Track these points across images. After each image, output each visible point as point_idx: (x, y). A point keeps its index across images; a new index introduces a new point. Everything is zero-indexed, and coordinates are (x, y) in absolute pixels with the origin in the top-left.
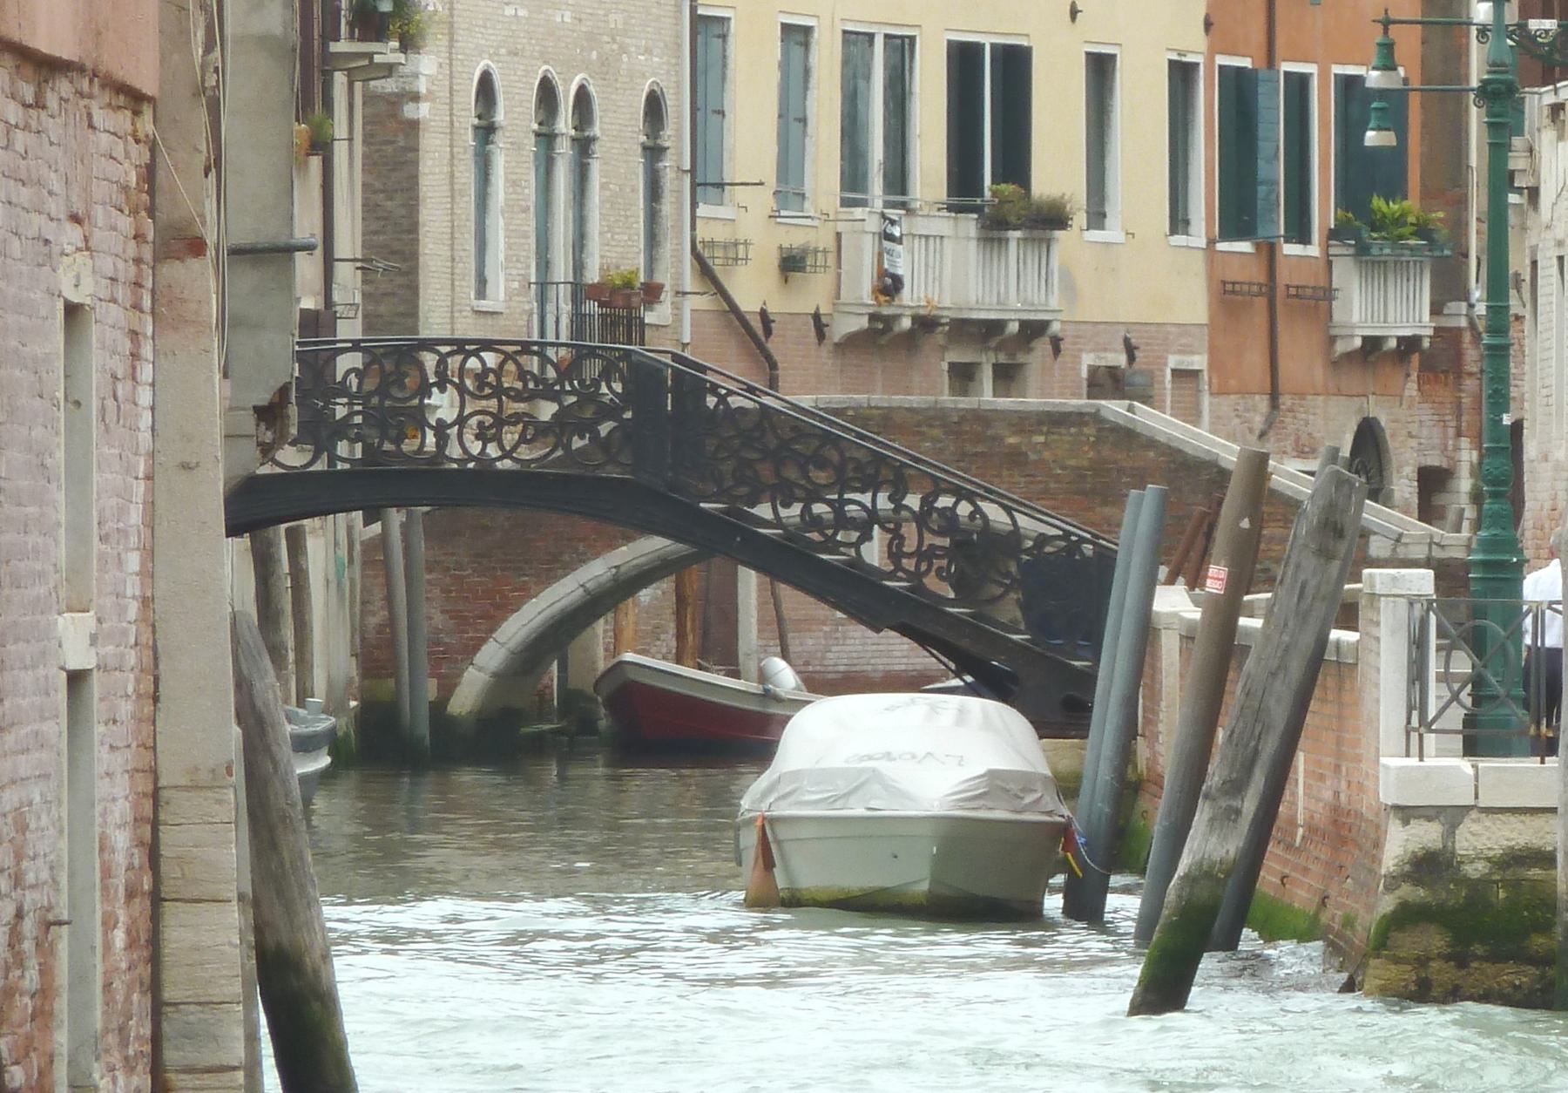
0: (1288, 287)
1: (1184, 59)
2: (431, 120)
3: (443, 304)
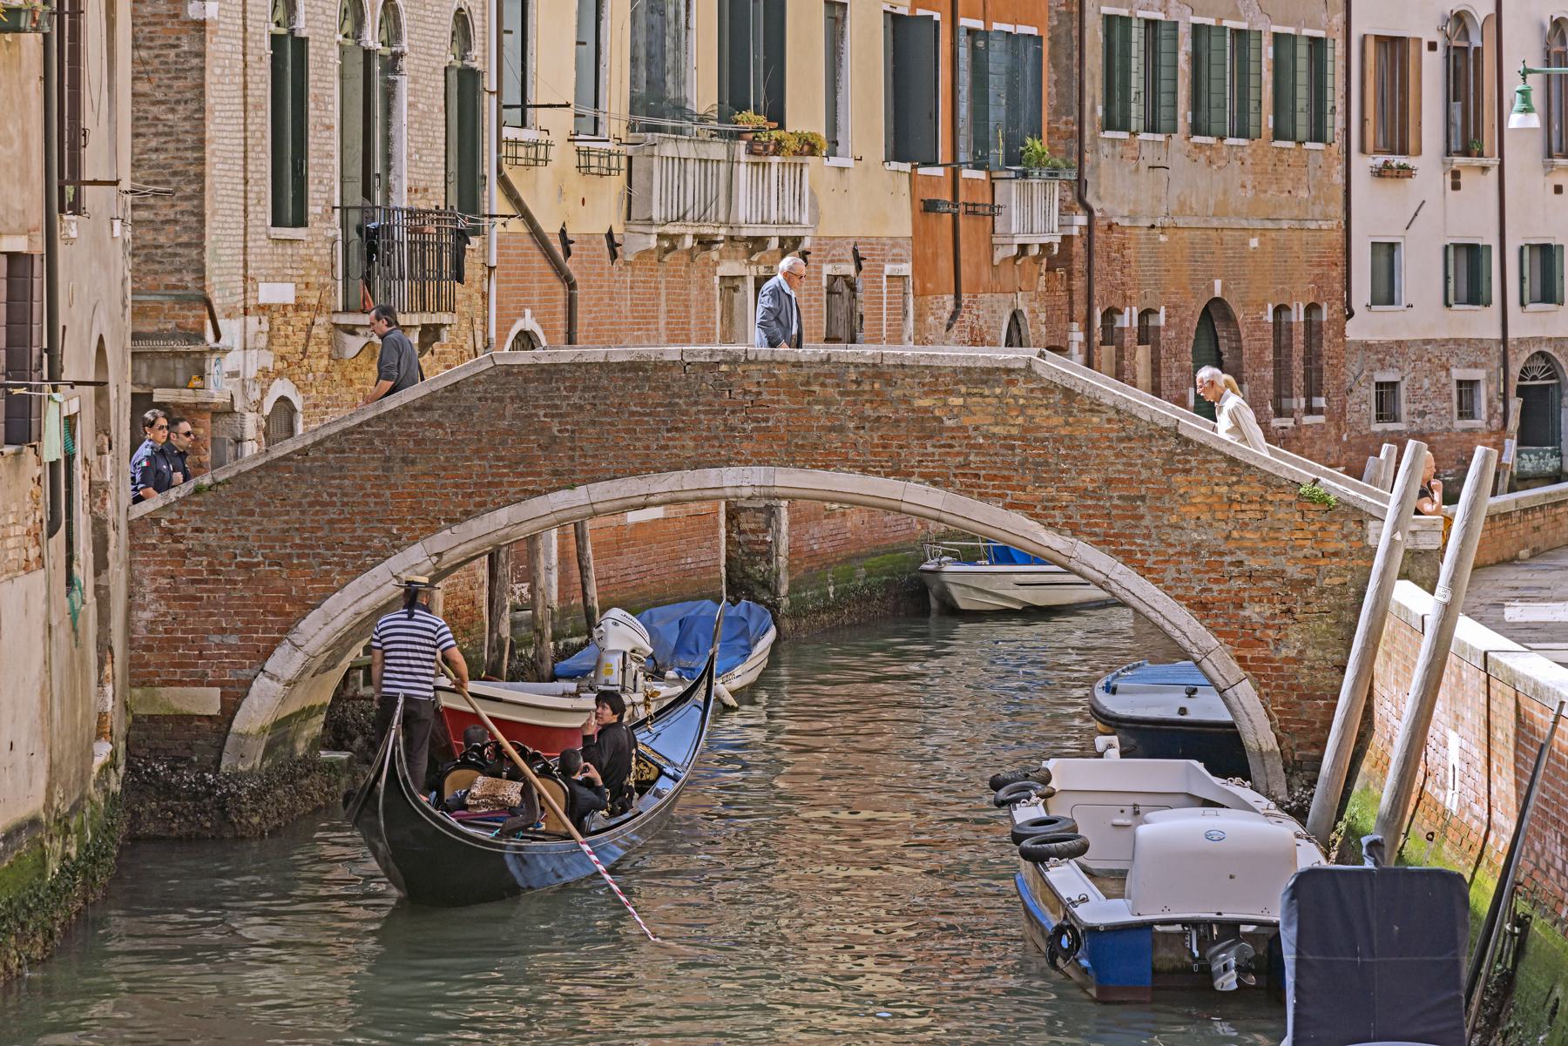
0: (967, 204)
1: (894, 11)
2: (218, 22)
3: (234, 232)
